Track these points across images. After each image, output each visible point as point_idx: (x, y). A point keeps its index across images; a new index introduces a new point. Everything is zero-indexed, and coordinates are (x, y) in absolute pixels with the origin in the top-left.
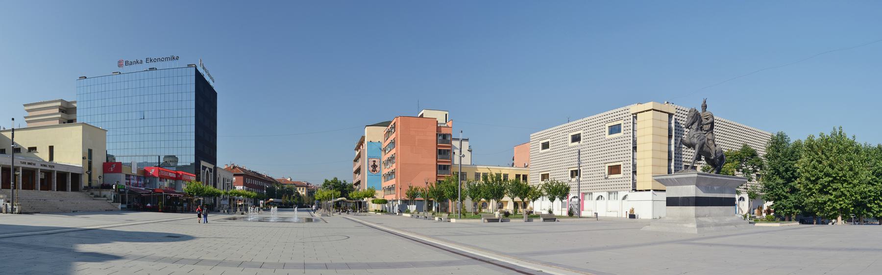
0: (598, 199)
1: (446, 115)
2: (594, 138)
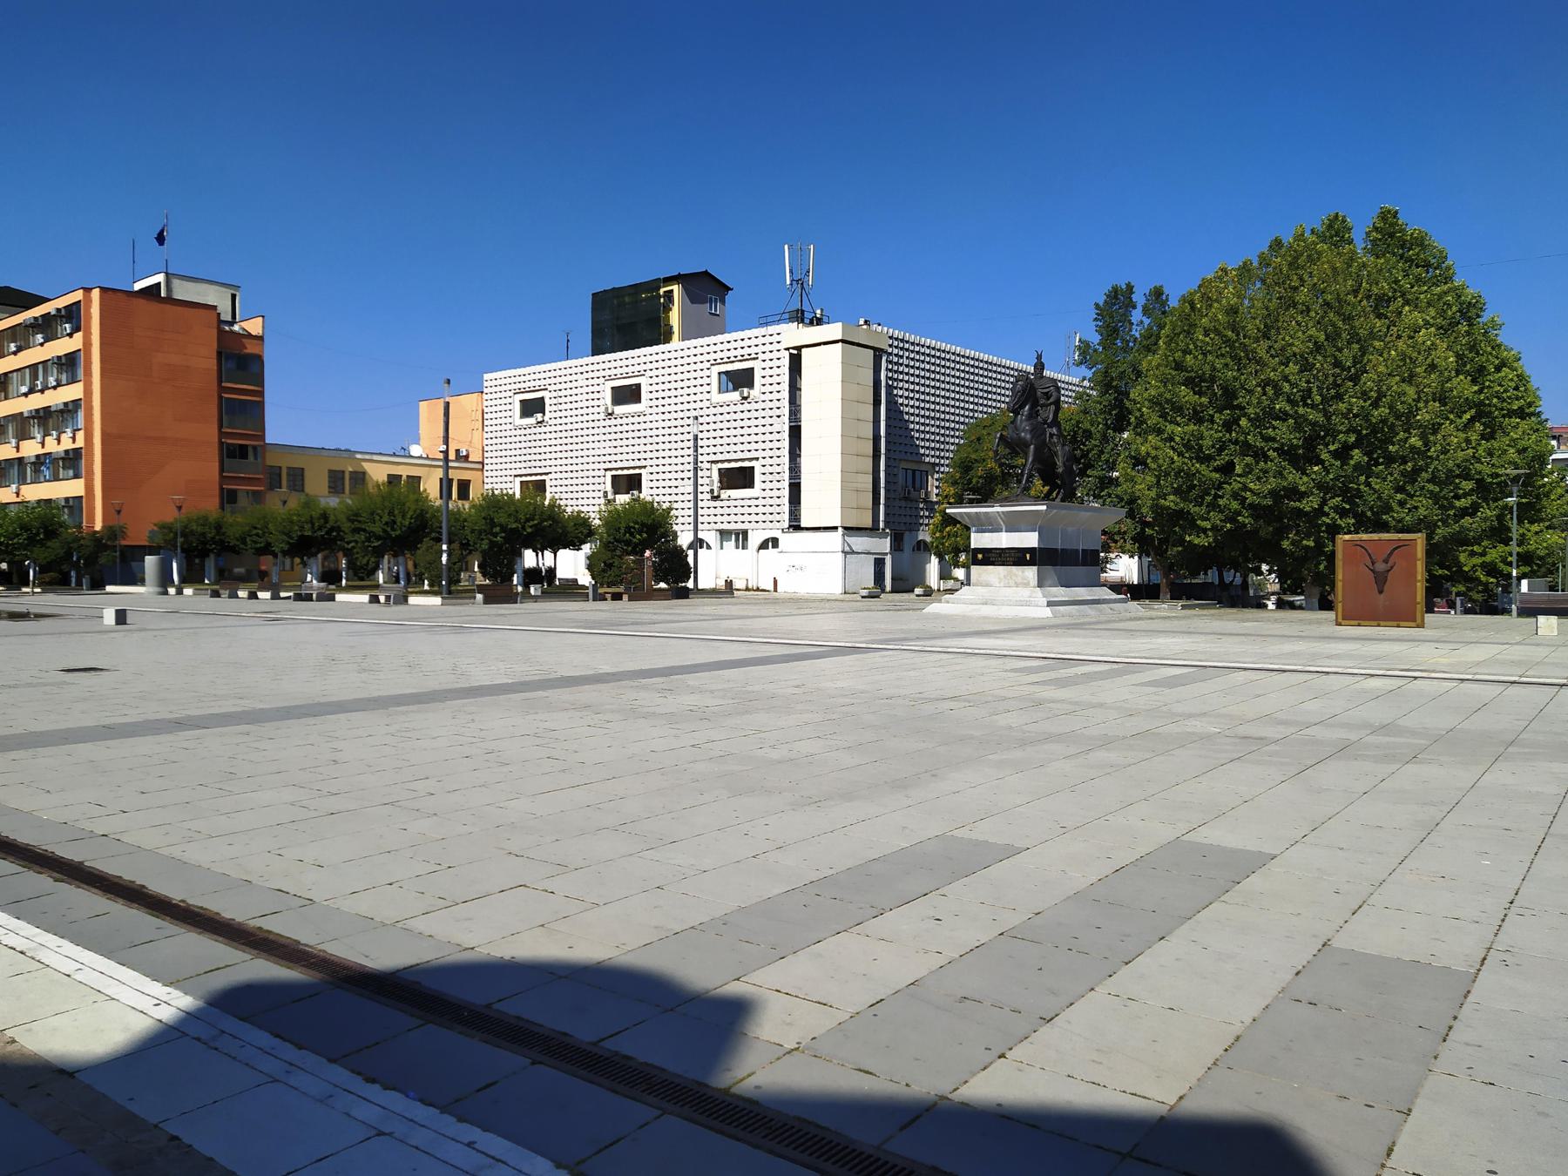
0: (764, 546)
2: (680, 400)
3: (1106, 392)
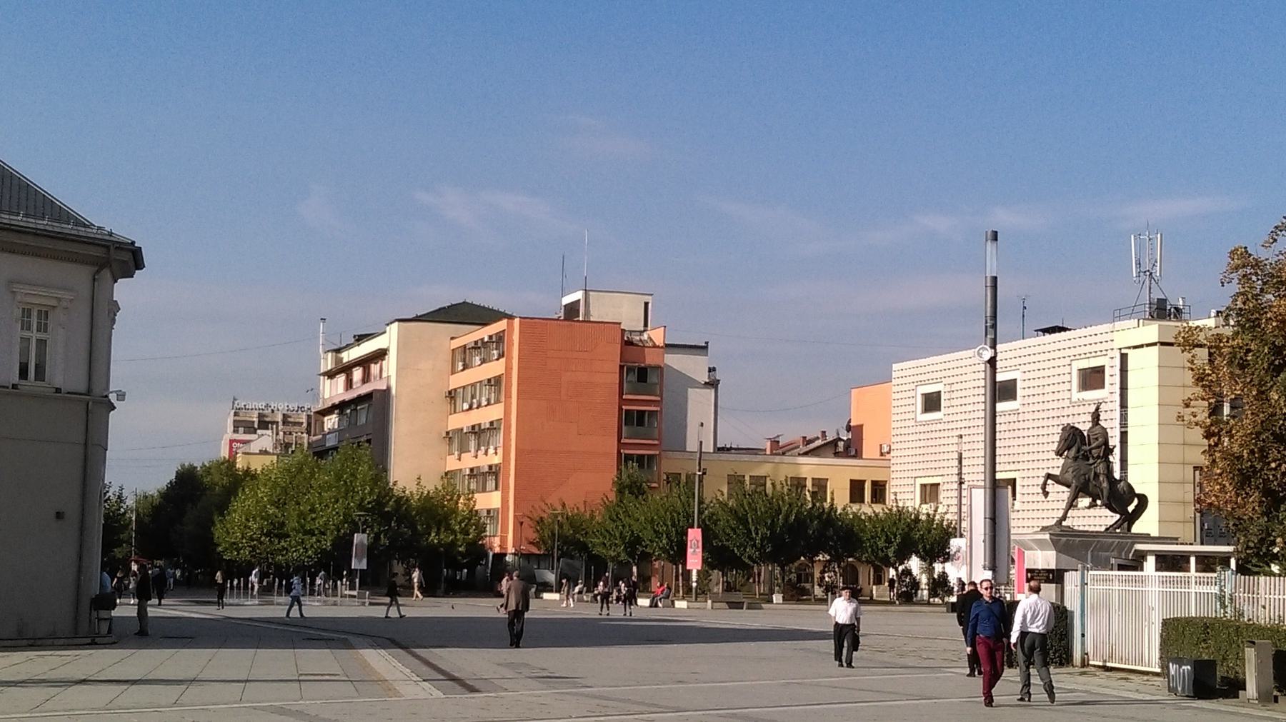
1: (646, 304)
3: (571, 525)
